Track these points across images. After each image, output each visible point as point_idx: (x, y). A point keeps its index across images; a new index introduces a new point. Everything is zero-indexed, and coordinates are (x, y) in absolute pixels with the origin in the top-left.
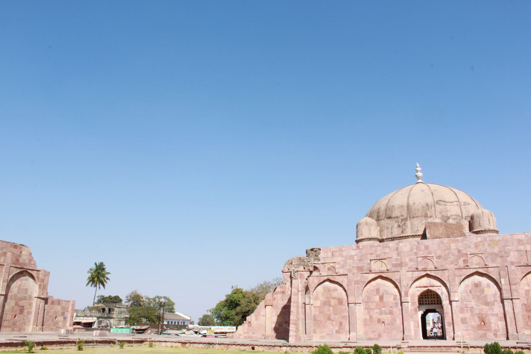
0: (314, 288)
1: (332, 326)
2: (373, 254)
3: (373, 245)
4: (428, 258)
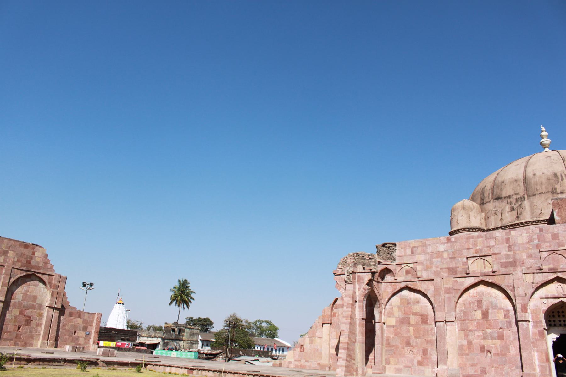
0: (387, 300)
1: (413, 355)
2: (472, 248)
3: (470, 235)
4: (558, 252)
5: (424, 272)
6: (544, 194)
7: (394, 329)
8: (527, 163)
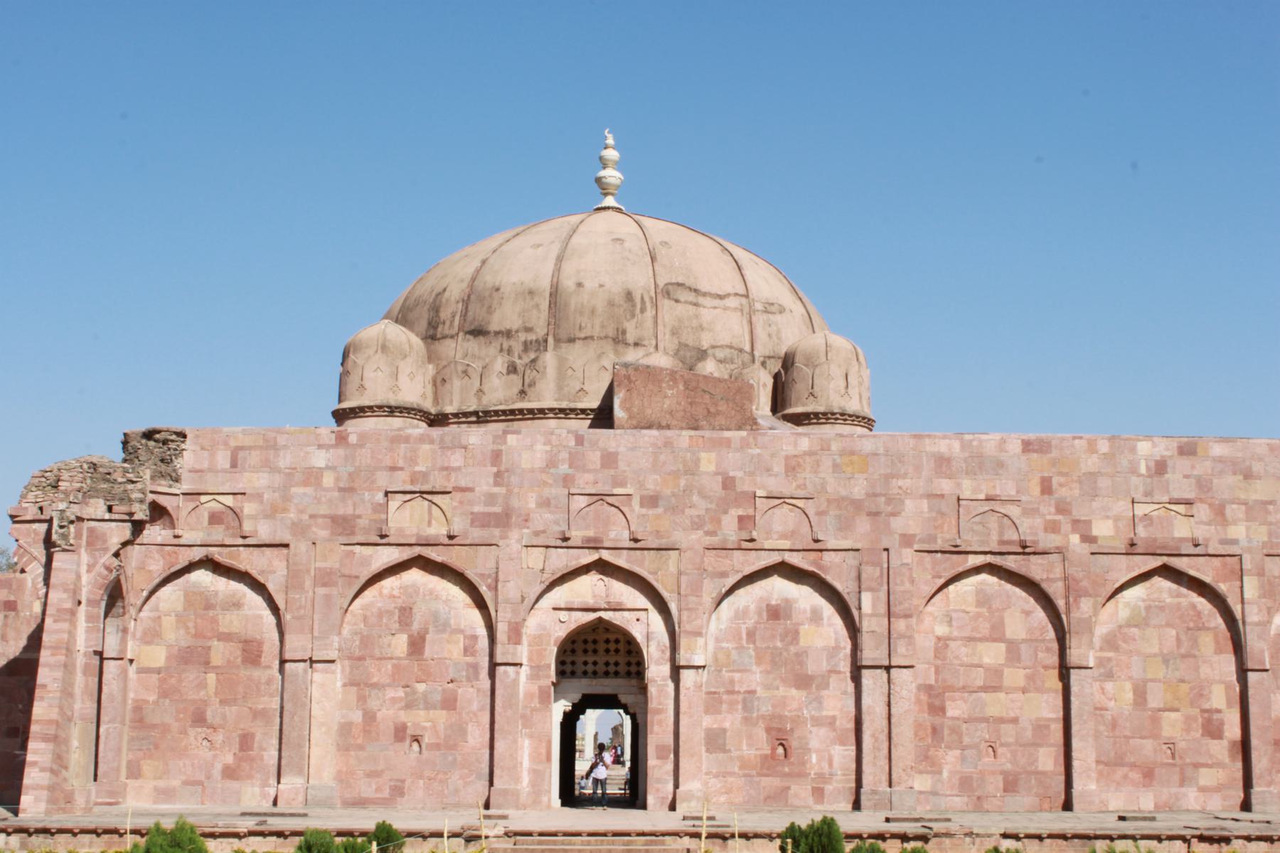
0: (145, 594)
2: (401, 469)
4: (609, 499)
5: (262, 521)
6: (596, 342)
7: (159, 679)
8: (566, 247)
